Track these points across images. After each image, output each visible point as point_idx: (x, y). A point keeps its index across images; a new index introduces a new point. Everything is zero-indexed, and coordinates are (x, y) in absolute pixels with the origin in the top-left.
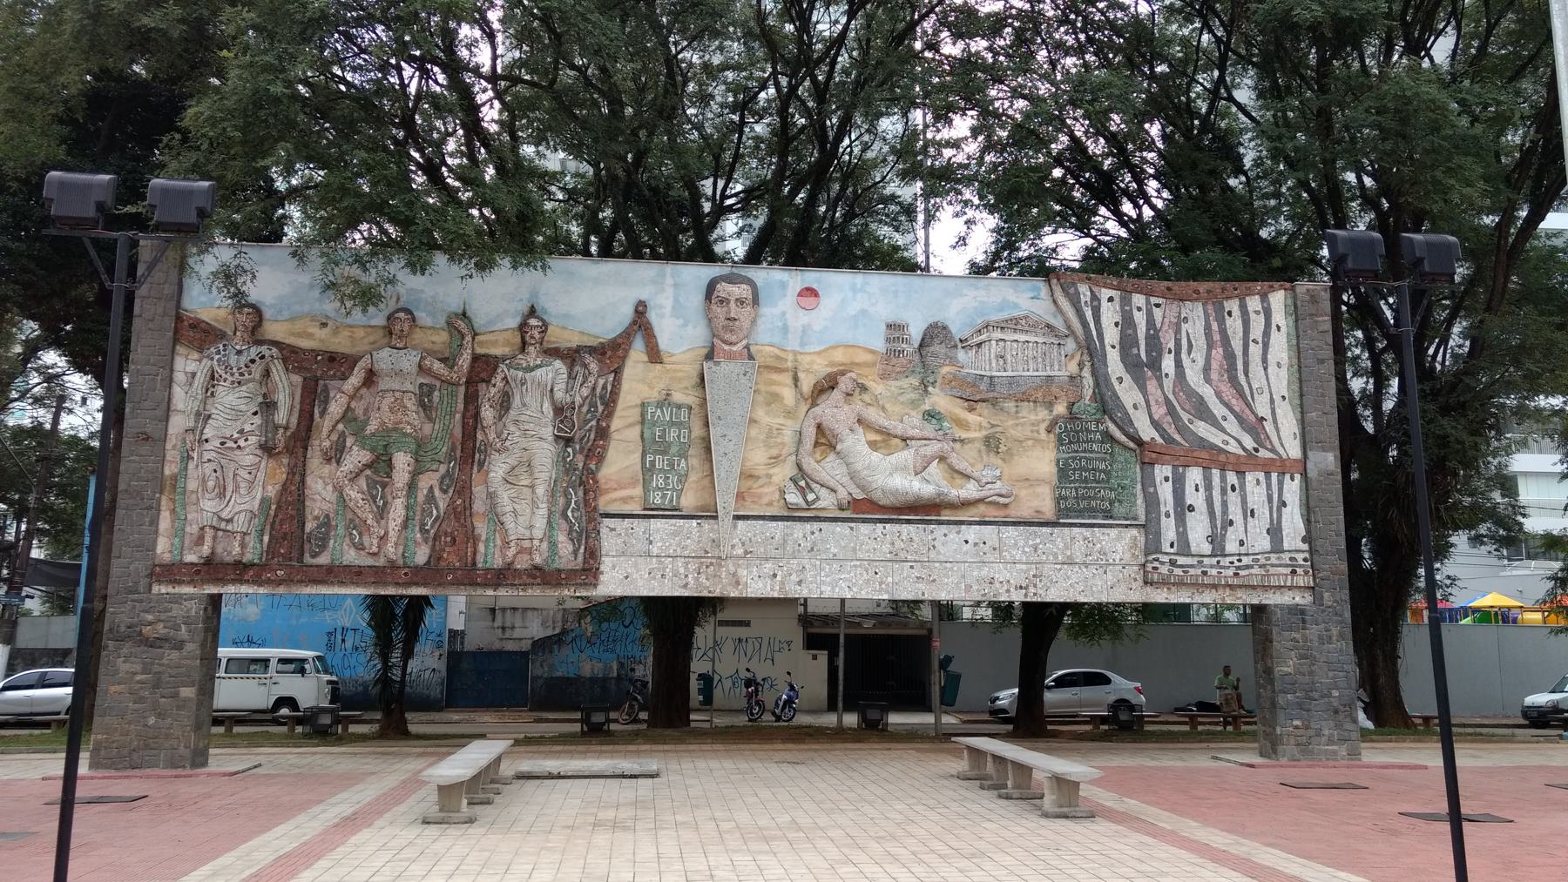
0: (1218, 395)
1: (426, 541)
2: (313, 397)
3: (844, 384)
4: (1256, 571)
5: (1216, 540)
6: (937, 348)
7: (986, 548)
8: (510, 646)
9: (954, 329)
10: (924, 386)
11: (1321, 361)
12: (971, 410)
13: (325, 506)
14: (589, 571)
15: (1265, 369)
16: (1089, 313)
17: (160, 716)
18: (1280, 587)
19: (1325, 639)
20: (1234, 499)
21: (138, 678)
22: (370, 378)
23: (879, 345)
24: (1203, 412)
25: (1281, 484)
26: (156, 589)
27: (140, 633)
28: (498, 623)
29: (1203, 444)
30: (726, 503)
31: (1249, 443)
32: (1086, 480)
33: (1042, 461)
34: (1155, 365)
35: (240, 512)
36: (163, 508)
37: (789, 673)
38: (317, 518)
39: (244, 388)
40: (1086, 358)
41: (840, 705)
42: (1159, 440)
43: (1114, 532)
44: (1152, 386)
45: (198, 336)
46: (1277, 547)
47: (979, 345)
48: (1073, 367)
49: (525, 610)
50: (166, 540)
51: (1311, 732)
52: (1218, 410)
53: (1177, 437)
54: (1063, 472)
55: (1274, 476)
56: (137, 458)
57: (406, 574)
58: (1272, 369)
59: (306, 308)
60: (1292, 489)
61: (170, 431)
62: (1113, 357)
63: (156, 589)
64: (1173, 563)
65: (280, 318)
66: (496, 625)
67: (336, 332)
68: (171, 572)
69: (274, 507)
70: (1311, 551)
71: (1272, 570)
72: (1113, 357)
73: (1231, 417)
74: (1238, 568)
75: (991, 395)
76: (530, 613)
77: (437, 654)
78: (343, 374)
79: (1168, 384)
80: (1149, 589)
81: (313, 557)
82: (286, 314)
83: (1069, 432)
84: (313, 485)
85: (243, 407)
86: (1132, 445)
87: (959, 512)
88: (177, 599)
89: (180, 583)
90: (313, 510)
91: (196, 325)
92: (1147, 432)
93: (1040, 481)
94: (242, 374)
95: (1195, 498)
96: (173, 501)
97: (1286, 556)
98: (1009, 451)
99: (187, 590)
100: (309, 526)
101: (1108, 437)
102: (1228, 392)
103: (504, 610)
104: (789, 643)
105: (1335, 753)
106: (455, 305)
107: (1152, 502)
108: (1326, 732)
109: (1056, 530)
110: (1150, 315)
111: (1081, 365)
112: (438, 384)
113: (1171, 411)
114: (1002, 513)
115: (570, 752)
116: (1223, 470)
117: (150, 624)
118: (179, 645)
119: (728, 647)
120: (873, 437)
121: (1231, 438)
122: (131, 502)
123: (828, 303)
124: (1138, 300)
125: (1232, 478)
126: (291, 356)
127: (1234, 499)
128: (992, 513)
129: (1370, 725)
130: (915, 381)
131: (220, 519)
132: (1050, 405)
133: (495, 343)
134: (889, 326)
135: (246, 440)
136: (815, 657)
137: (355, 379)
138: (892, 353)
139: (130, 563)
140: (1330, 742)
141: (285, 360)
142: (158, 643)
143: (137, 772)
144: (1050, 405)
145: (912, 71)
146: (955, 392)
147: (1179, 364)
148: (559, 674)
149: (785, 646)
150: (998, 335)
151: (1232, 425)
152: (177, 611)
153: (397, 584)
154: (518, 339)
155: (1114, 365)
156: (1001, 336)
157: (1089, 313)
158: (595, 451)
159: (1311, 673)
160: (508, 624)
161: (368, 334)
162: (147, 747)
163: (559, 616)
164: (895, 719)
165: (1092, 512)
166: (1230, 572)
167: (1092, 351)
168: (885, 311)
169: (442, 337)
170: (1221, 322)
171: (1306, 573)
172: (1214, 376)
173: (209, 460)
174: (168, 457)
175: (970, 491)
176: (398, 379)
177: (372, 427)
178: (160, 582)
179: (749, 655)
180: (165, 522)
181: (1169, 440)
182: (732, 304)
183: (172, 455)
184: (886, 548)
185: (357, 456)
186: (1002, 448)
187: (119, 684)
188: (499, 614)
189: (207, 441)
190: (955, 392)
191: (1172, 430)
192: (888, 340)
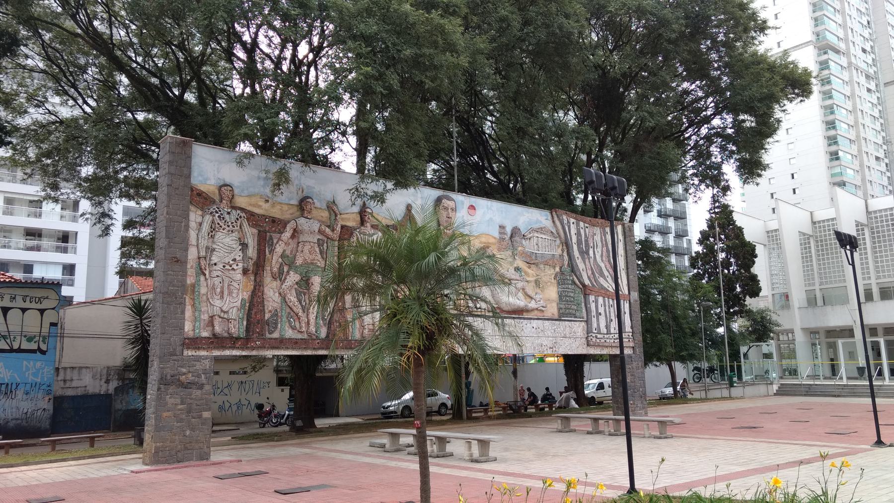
0: (606, 266)
1: (325, 325)
2: (264, 242)
6: (517, 238)
8: (70, 393)
9: (522, 230)
10: (514, 256)
12: (529, 268)
13: (275, 305)
16: (567, 228)
17: (193, 430)
21: (180, 407)
22: (296, 233)
23: (497, 235)
26: (186, 353)
27: (179, 380)
28: (61, 377)
29: (602, 287)
32: (567, 301)
33: (552, 292)
35: (233, 307)
36: (187, 304)
37: (268, 398)
38: (270, 311)
39: (234, 234)
40: (565, 247)
41: (112, 429)
43: (577, 323)
44: (587, 261)
45: (202, 200)
48: (559, 251)
49: (81, 368)
50: (190, 323)
54: (560, 297)
56: (172, 273)
57: (318, 343)
59: (257, 190)
61: (189, 257)
62: (575, 247)
63: (186, 353)
64: (596, 337)
65: (243, 195)
66: (59, 378)
67: (273, 205)
68: (195, 342)
69: (247, 305)
72: (575, 247)
75: (536, 261)
76: (84, 370)
77: (47, 399)
78: (280, 230)
81: (270, 333)
82: (246, 193)
83: (561, 278)
84: (268, 293)
85: (234, 246)
86: (581, 286)
87: (529, 314)
88: (198, 359)
89: (199, 349)
90: (268, 306)
91: (200, 194)
92: (587, 282)
93: (553, 301)
94: (233, 227)
95: (601, 310)
96: (193, 299)
99: (203, 353)
100: (267, 316)
101: (574, 283)
103: (65, 369)
104: (268, 383)
106: (329, 198)
107: (588, 311)
109: (561, 322)
110: (585, 231)
111: (563, 251)
112: (326, 239)
113: (593, 273)
114: (542, 315)
115: (332, 440)
117: (184, 374)
118: (201, 387)
119: (235, 386)
122: (169, 299)
123: (479, 212)
126: (251, 217)
128: (540, 315)
129: (577, 406)
130: (509, 253)
131: (222, 311)
132: (554, 267)
133: (348, 220)
134: (500, 227)
135: (237, 265)
136: (283, 390)
137: (287, 234)
138: (502, 239)
139: (171, 337)
141: (248, 219)
142: (189, 386)
143: (181, 464)
144: (554, 267)
146: (524, 259)
147: (594, 252)
148: (132, 407)
149: (267, 385)
150: (536, 234)
152: (198, 366)
153: (314, 349)
154: (359, 219)
155: (576, 253)
156: (537, 235)
157: (567, 228)
160: (68, 378)
161: (289, 209)
162: (186, 449)
163: (105, 372)
164: (320, 423)
165: (570, 315)
166: (612, 341)
167: (567, 244)
168: (498, 220)
169: (326, 214)
170: (605, 237)
172: (604, 259)
173: (218, 276)
174: (189, 273)
175: (532, 305)
176: (312, 236)
177: (299, 261)
178: (188, 348)
179: (246, 390)
180: (188, 313)
181: (593, 285)
182: (450, 211)
183: (191, 272)
185: (293, 278)
186: (541, 286)
187: (168, 411)
188: (61, 372)
189: (215, 264)
190: (524, 259)
192: (500, 233)
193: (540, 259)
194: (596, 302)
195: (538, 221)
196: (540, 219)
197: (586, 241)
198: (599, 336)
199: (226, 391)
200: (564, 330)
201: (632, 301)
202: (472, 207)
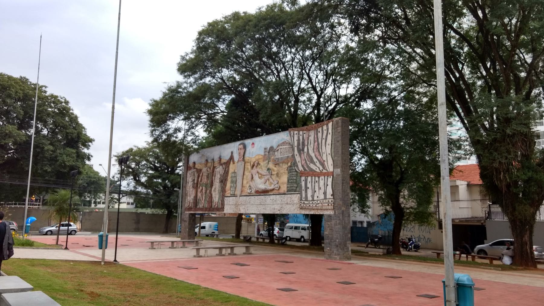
0: (315, 155)
3: (256, 164)
4: (320, 205)
5: (313, 196)
7: (274, 201)
11: (338, 141)
14: (223, 209)
15: (325, 146)
18: (326, 209)
19: (336, 225)
20: (317, 184)
24: (312, 161)
25: (327, 179)
29: (312, 170)
30: (238, 192)
31: (321, 168)
33: (284, 178)
34: (303, 150)
42: (303, 170)
44: (302, 155)
46: (325, 198)
47: (278, 150)
51: (331, 252)
52: (315, 160)
53: (307, 169)
55: (326, 177)
58: (327, 146)
60: (330, 180)
62: (296, 149)
64: (304, 203)
70: (334, 198)
71: (324, 204)
73: (318, 162)
74: (317, 204)
79: (305, 154)
80: (301, 210)
83: (290, 170)
93: (285, 183)
95: (309, 185)
97: (327, 200)
98: (280, 177)
102: (317, 154)
105: (336, 258)
108: (335, 252)
109: (285, 195)
116: (315, 177)
120: (260, 176)
121: (316, 167)
124: (301, 133)
125: (317, 179)
127: (317, 184)
132: (288, 163)
140: (335, 255)
145: (251, 94)
151: (318, 164)
158: (225, 185)
159: (332, 234)
166: (314, 205)
168: (264, 146)
170: (317, 135)
171: (331, 205)
172: (315, 150)
184: (259, 202)
191: (305, 167)
193: (280, 161)
194: (306, 181)
195: (283, 139)
196: (283, 137)
197: (303, 143)
198: (306, 202)
199: (412, 230)
200: (287, 200)
201: (334, 176)
202: (253, 144)
